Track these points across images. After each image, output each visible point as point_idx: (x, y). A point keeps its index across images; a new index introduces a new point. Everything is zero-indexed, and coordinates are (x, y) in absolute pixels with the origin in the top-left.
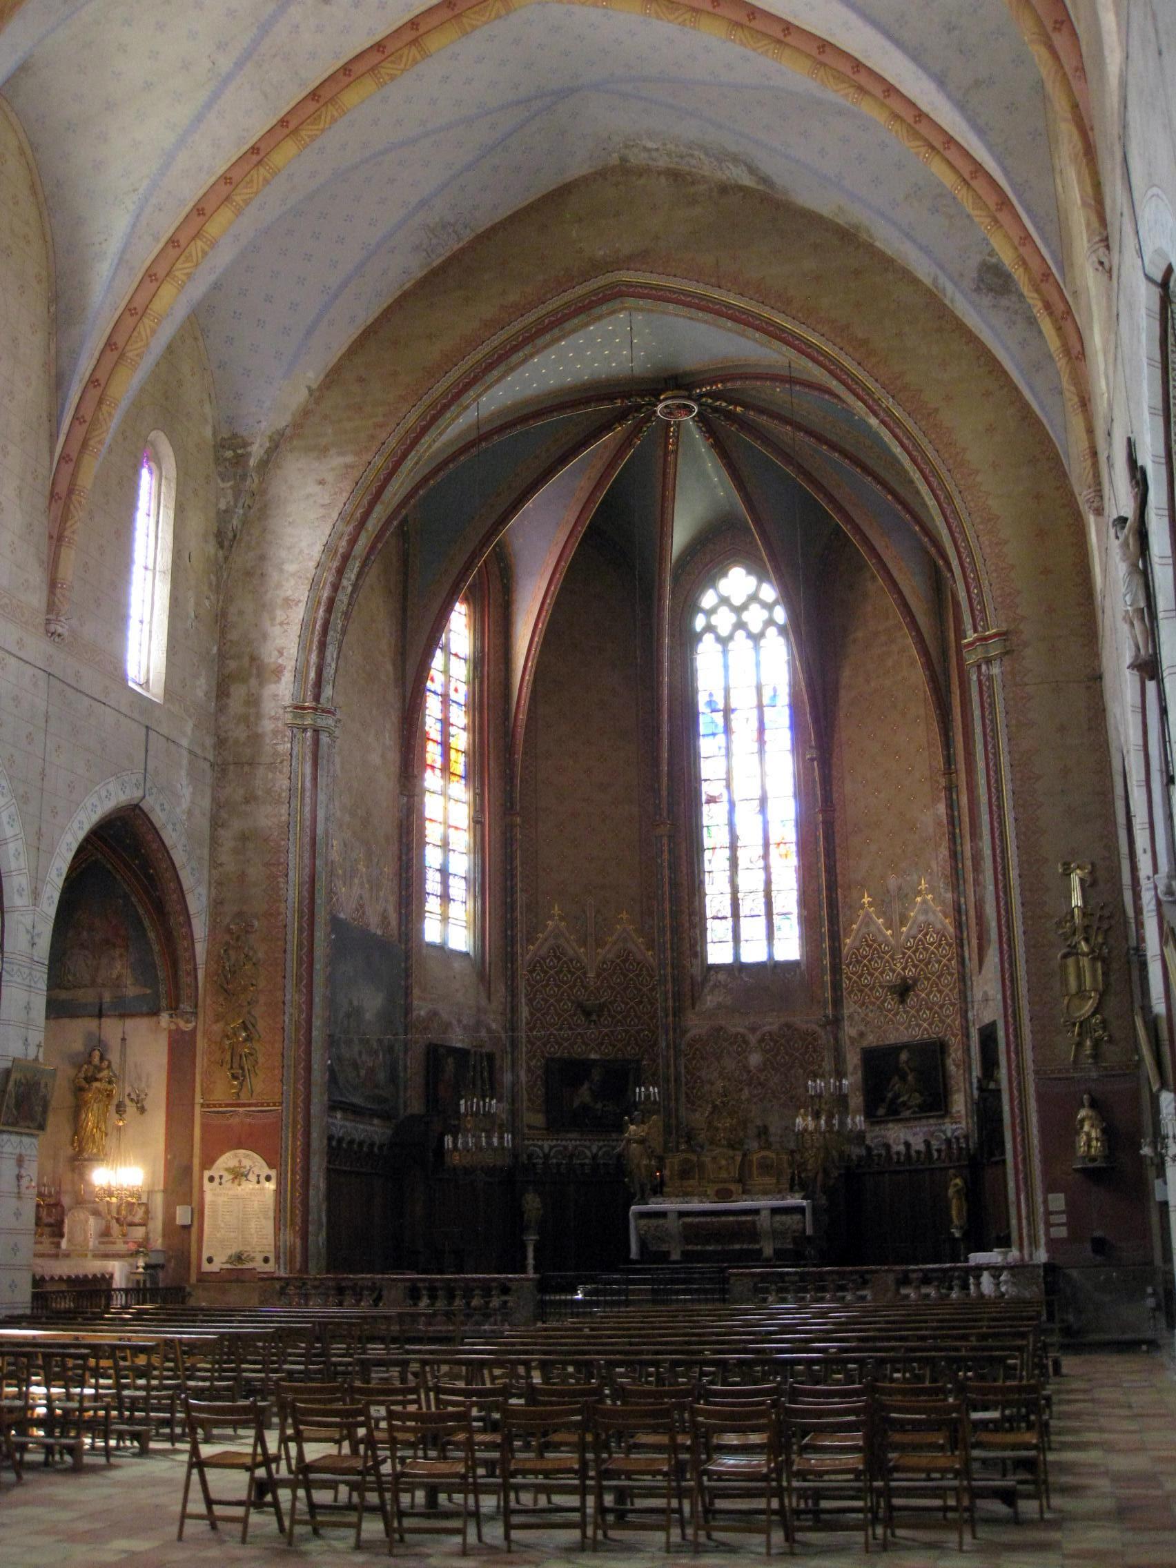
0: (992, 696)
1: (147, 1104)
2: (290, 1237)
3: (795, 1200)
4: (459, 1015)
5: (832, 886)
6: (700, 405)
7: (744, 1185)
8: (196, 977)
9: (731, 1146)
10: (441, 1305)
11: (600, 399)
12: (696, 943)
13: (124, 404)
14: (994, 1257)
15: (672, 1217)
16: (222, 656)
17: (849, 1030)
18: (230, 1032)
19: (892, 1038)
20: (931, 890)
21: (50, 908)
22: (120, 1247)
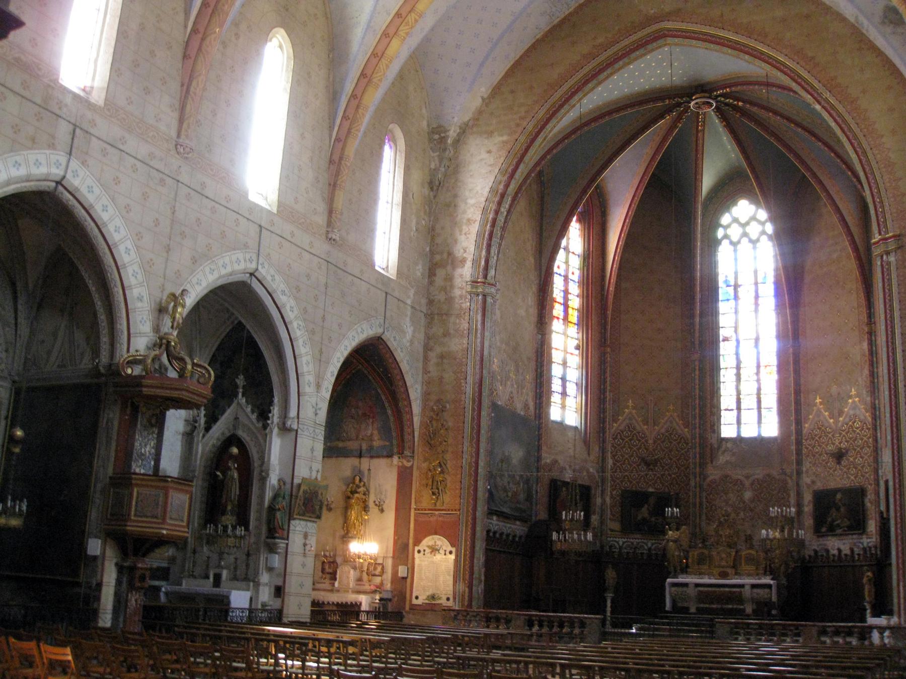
0: (890, 274)
1: (385, 507)
2: (462, 587)
3: (767, 580)
4: (570, 463)
5: (797, 392)
6: (717, 102)
7: (736, 569)
8: (414, 437)
9: (730, 546)
10: (545, 630)
11: (655, 100)
12: (714, 425)
13: (372, 109)
14: (882, 621)
15: (691, 587)
16: (432, 253)
17: (806, 480)
18: (432, 468)
19: (832, 485)
20: (857, 395)
21: (326, 394)
22: (367, 587)
